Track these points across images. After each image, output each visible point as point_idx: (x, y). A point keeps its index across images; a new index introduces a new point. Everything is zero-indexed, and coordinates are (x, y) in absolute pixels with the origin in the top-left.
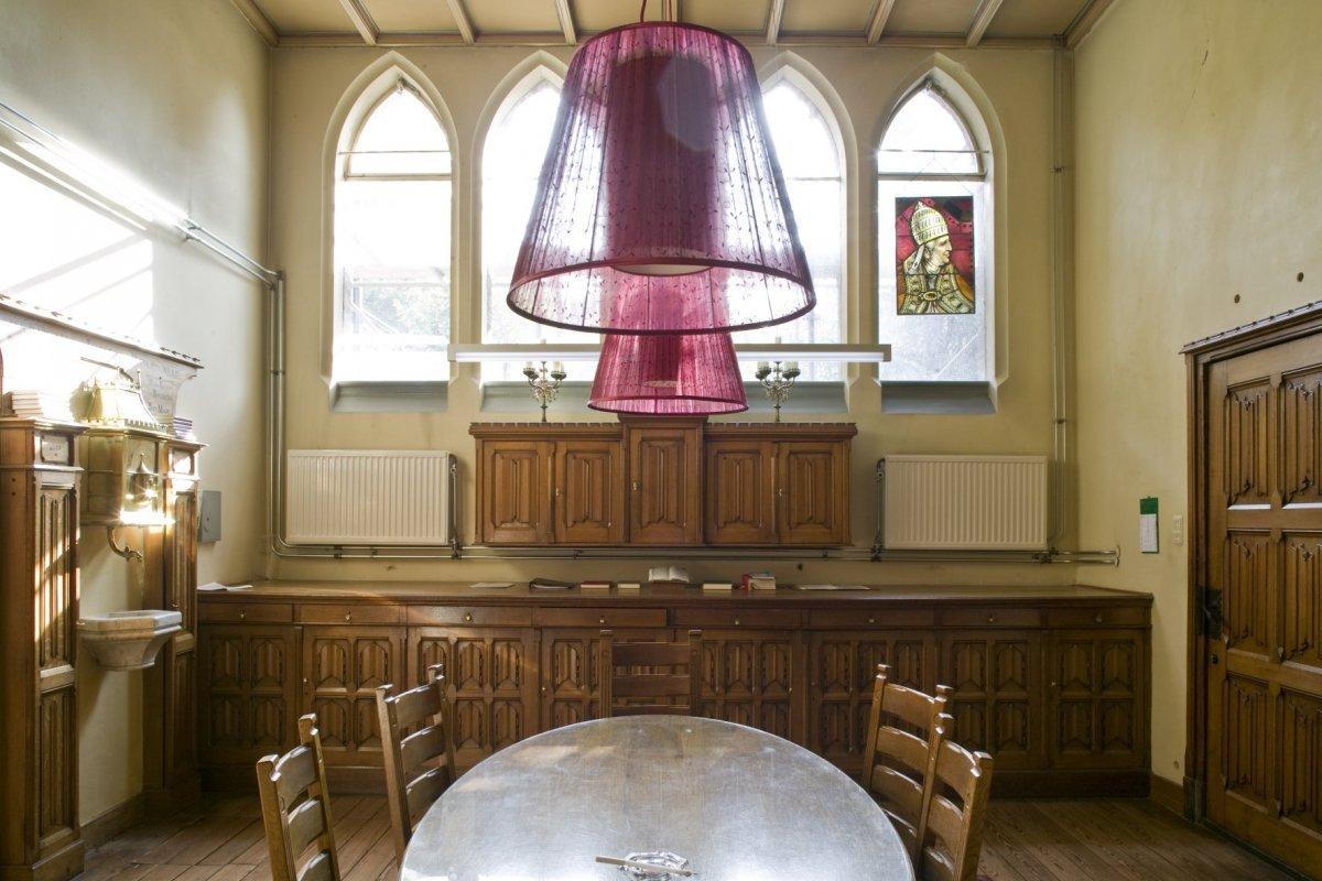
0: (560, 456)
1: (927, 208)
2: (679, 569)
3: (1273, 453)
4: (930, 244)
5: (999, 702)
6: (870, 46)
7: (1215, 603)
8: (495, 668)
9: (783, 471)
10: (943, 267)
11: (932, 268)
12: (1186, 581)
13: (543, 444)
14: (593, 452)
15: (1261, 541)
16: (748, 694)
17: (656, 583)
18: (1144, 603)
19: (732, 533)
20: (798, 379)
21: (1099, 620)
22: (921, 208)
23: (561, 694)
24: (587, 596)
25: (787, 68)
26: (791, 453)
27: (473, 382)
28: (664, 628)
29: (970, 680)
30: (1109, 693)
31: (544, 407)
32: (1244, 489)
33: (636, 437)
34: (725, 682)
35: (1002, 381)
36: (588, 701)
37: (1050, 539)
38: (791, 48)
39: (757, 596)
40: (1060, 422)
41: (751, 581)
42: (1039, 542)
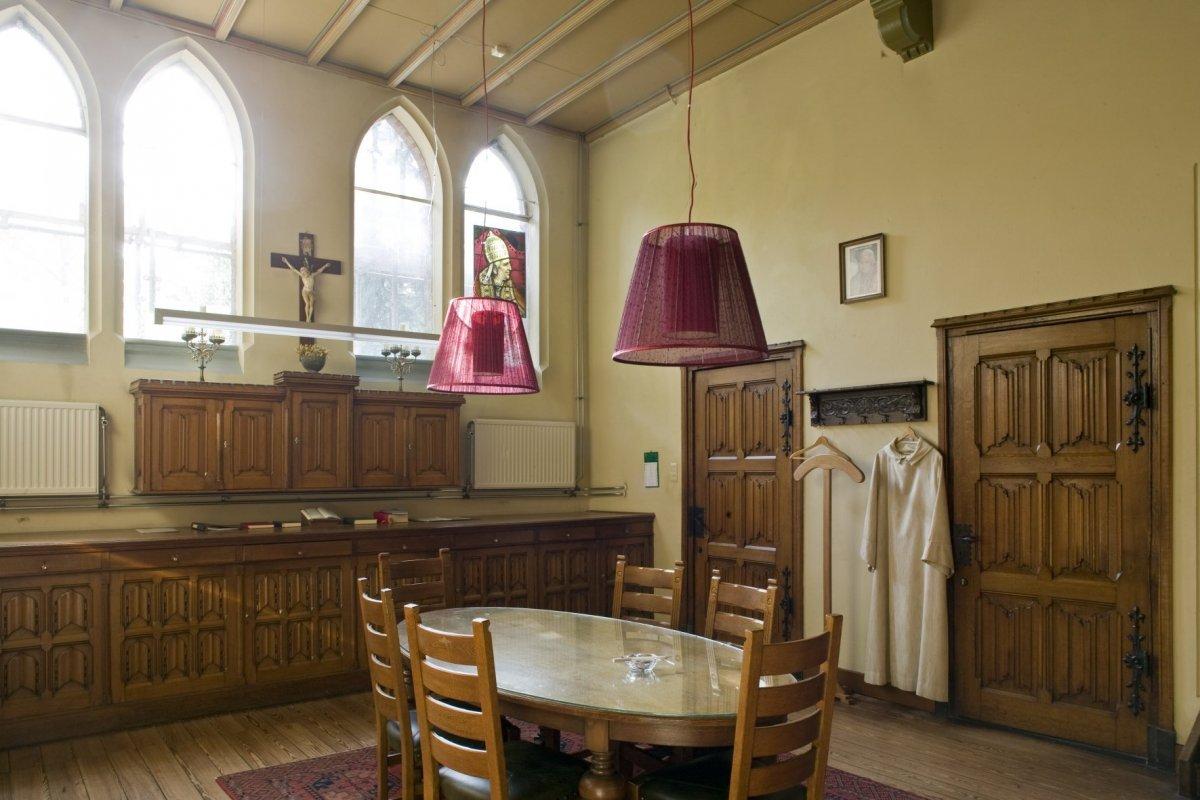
0: (228, 412)
1: (496, 237)
2: (328, 509)
3: (738, 427)
4: (497, 264)
5: (548, 594)
6: (309, 65)
7: (700, 516)
8: (200, 603)
9: (228, 425)
10: (505, 281)
11: (498, 281)
12: (680, 503)
13: (211, 401)
14: (383, 414)
15: (732, 478)
16: (148, 629)
17: (315, 521)
18: (649, 519)
19: (373, 479)
20: (419, 358)
21: (627, 531)
22: (491, 235)
23: (260, 618)
24: (289, 531)
25: (400, 107)
26: (235, 409)
27: (117, 339)
28: (349, 556)
29: (555, 578)
30: (293, 615)
31: (202, 368)
32: (719, 447)
33: (298, 398)
34: (318, 601)
35: (94, 334)
36: (286, 622)
37: (577, 481)
38: (405, 95)
39: (396, 527)
40: (580, 398)
41: (390, 516)
42: (570, 482)
